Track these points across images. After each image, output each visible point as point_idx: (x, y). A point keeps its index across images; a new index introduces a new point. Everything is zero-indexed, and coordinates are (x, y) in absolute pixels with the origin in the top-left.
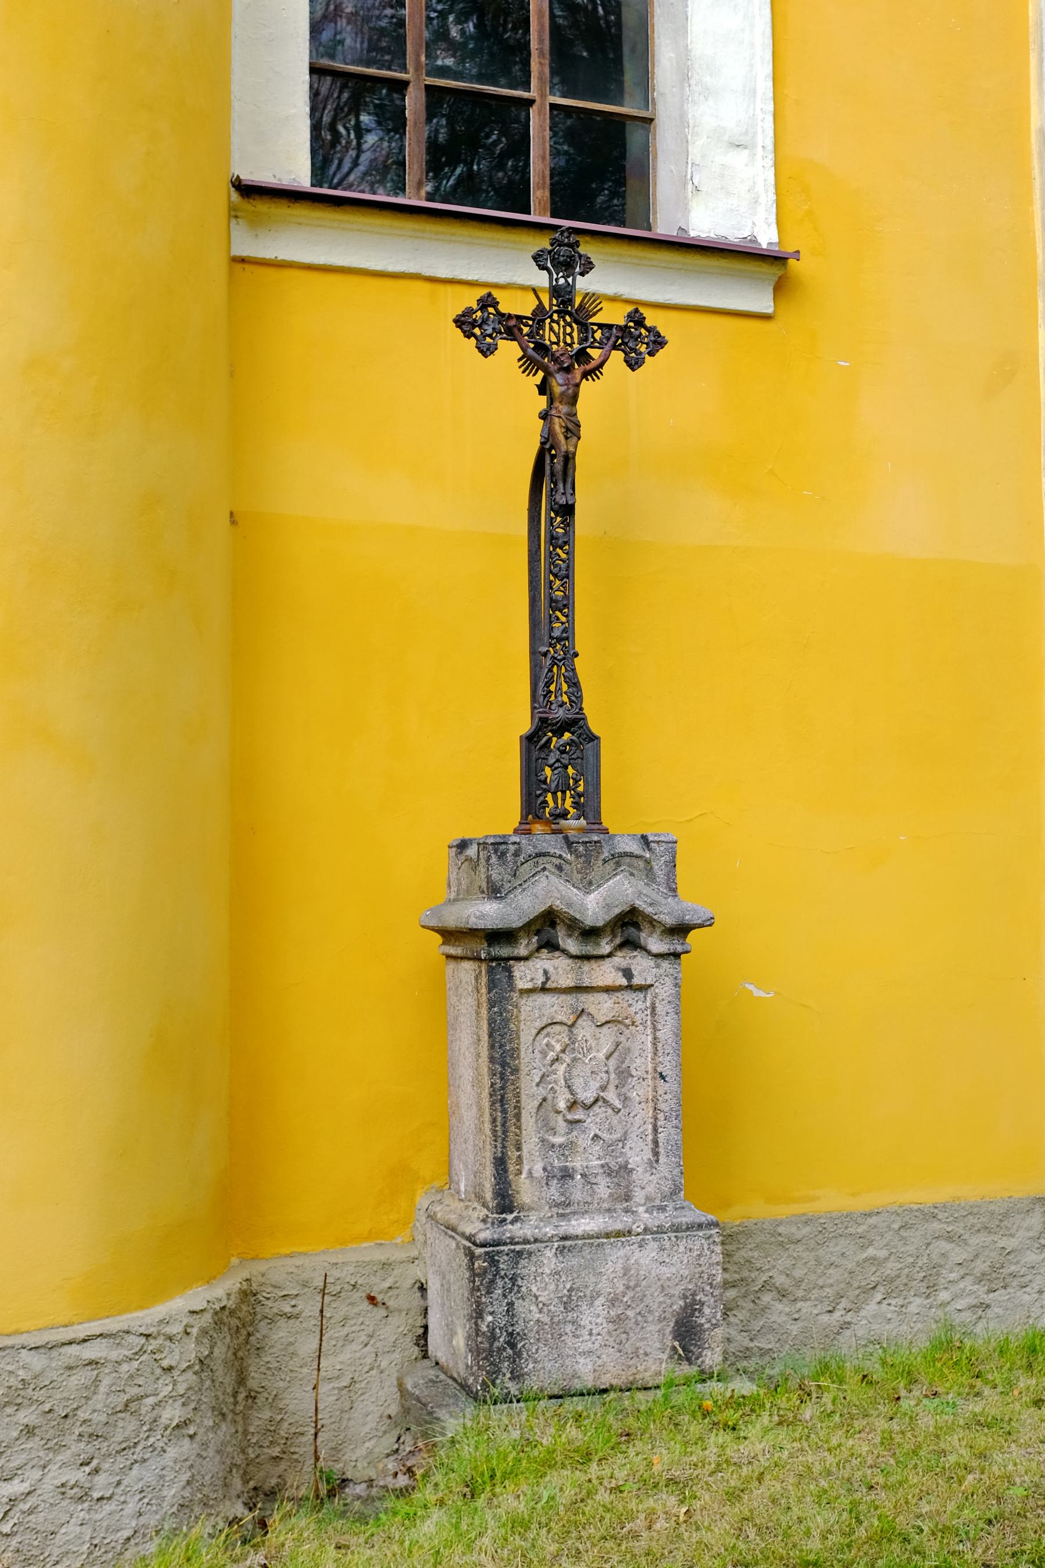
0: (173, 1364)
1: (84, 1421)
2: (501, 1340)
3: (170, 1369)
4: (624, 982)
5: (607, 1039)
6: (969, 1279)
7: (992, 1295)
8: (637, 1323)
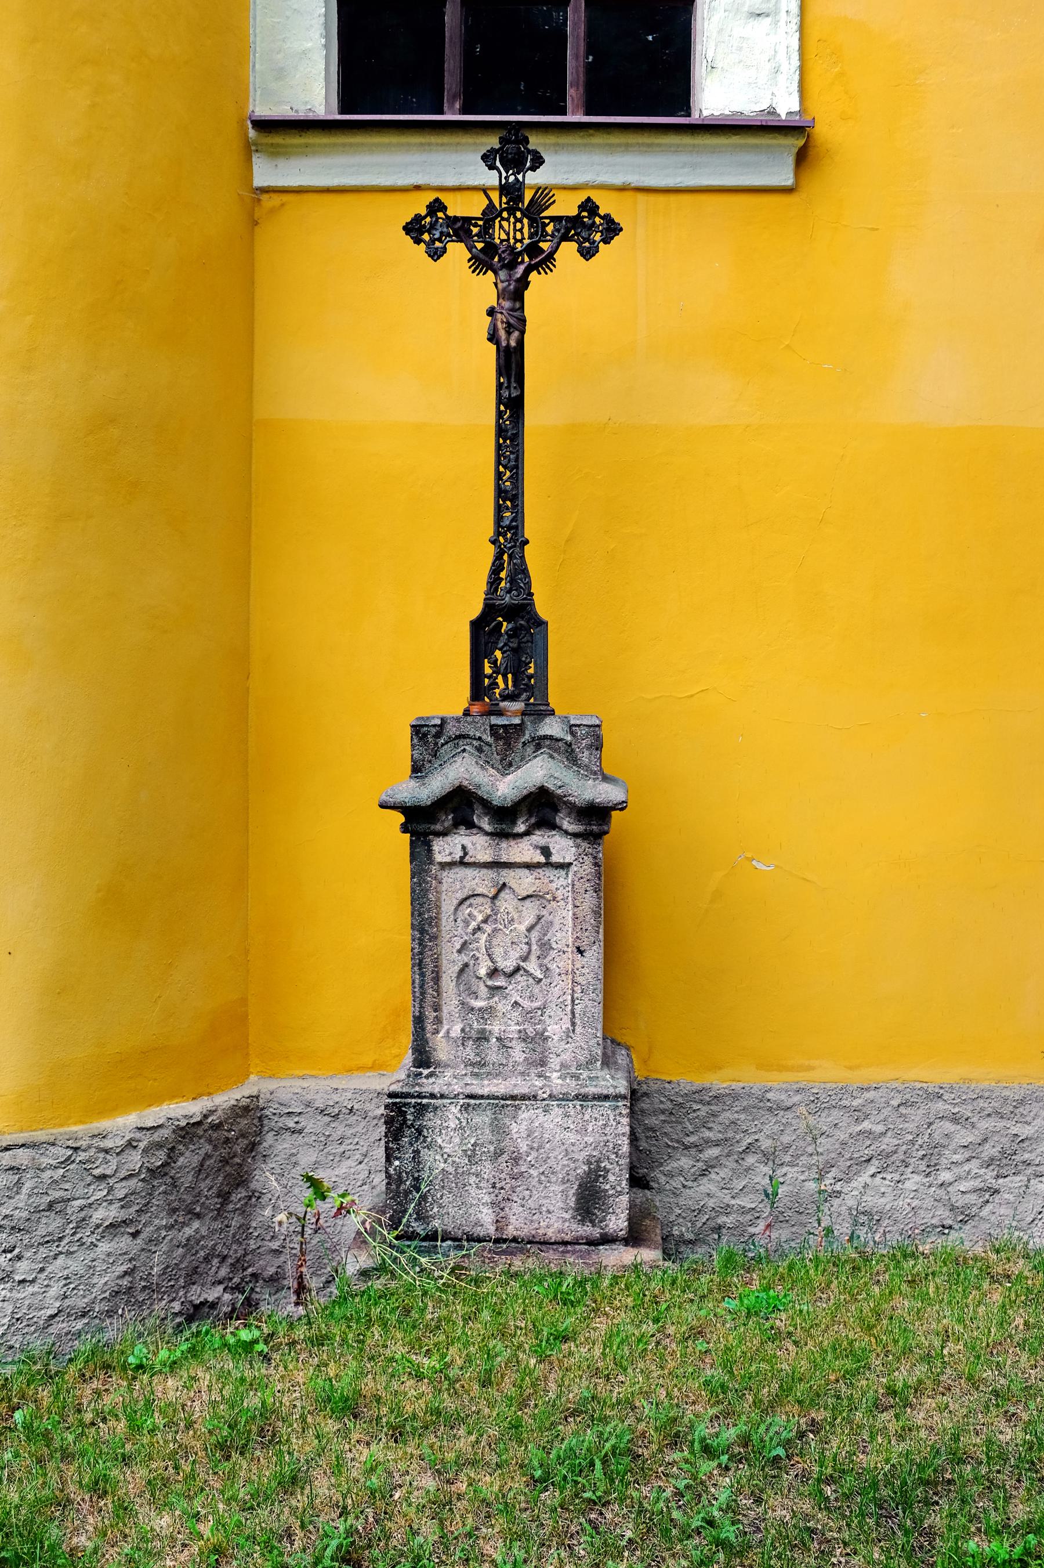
0: (108, 1172)
1: (6, 1216)
2: (408, 1183)
3: (103, 1177)
4: (542, 859)
5: (529, 912)
6: (975, 1163)
7: (1001, 1181)
8: (540, 1182)
